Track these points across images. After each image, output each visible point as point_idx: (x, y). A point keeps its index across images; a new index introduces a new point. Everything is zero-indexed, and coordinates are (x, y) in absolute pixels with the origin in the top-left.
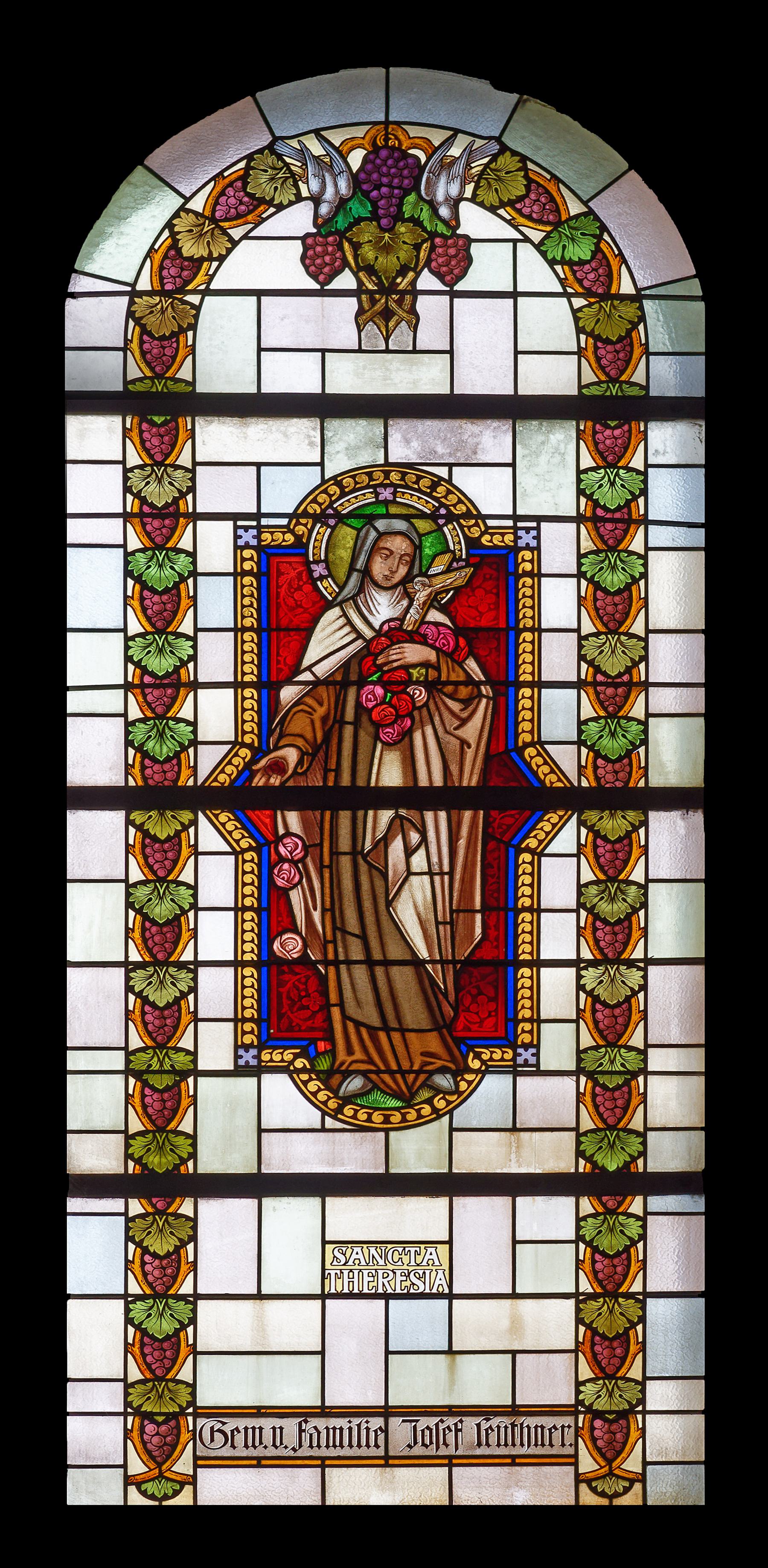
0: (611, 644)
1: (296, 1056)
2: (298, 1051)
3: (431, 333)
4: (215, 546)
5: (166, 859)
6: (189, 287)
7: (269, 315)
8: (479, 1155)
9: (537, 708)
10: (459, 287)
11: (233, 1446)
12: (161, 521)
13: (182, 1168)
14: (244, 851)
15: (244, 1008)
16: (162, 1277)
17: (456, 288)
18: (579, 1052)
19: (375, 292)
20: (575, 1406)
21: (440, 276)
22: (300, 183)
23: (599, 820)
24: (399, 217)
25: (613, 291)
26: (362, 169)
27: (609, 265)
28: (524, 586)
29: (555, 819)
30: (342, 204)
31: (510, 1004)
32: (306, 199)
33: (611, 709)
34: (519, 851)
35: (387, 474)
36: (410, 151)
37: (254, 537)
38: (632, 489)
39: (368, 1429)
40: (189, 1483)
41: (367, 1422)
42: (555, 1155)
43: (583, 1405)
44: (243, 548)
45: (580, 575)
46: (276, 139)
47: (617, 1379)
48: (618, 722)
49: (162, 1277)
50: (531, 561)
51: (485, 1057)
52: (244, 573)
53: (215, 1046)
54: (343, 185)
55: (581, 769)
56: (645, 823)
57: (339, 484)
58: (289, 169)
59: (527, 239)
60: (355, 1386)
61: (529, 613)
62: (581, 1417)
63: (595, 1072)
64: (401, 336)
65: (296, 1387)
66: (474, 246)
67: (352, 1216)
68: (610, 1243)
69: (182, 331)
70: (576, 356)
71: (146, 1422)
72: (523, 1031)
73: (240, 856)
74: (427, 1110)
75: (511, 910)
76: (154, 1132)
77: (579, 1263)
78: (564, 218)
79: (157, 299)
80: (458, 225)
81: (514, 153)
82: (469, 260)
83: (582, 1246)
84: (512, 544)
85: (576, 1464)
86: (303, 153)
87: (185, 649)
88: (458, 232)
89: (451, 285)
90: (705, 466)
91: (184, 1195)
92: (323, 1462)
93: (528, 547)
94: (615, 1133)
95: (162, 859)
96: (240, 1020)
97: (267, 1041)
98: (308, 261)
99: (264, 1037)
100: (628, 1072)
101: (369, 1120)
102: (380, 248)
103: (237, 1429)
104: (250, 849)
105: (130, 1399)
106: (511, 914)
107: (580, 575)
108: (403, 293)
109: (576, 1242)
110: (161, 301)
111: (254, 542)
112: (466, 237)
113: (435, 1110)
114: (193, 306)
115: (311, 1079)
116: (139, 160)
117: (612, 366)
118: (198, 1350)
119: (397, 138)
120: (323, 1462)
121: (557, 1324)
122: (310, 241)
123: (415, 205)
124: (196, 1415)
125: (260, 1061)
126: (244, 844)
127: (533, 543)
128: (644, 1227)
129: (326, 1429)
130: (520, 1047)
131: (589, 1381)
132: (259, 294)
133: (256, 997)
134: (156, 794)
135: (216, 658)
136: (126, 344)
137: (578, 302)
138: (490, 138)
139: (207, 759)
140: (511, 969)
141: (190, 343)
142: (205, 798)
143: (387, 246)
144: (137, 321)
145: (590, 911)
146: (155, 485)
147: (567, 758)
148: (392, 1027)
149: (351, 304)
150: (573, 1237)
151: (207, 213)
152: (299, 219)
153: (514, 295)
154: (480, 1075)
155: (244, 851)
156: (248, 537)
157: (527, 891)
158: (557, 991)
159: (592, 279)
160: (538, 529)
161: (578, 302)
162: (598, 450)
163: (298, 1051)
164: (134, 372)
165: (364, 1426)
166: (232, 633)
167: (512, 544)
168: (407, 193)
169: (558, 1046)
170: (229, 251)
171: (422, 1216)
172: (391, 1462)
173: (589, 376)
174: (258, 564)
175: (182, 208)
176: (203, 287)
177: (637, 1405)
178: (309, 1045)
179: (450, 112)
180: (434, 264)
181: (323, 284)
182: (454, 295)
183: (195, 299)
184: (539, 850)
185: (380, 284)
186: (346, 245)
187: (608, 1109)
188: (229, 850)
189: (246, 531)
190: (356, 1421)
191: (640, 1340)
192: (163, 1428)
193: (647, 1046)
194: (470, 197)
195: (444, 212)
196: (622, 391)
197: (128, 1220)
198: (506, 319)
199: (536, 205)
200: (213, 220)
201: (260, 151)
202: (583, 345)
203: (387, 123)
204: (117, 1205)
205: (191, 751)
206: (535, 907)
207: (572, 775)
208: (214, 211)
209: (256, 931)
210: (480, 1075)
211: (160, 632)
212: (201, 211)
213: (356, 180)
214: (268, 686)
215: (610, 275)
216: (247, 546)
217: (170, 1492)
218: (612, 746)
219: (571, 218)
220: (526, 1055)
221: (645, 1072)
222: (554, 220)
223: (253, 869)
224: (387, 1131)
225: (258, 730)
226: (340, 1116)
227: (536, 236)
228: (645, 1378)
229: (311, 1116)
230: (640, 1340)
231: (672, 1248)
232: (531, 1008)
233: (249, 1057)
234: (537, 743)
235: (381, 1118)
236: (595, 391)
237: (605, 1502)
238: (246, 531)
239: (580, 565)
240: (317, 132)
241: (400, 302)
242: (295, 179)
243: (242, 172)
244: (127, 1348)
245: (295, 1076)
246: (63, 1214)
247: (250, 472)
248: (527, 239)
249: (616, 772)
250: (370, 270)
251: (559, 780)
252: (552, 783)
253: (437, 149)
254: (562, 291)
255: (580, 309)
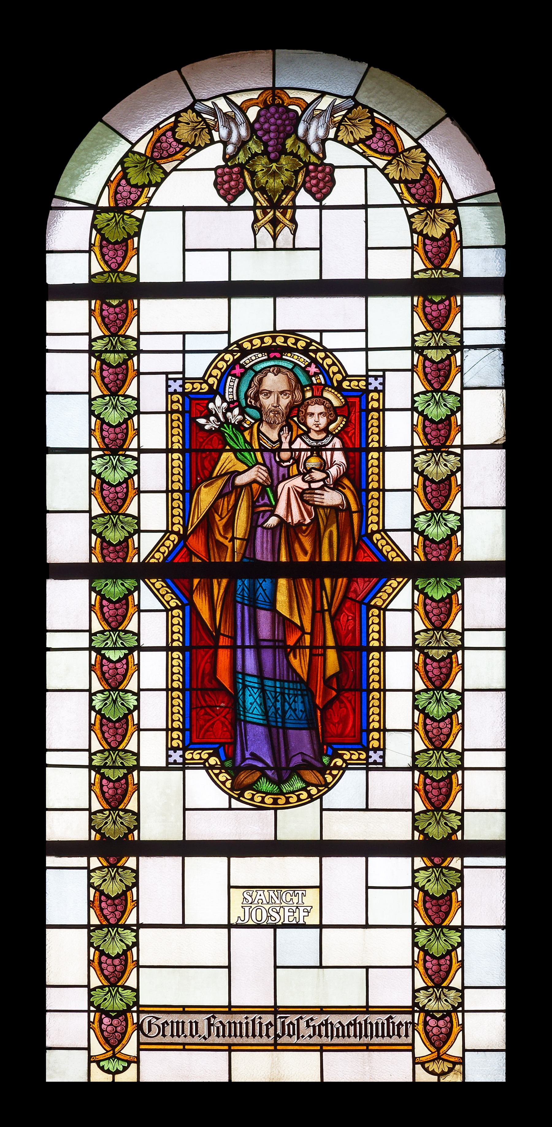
0: (436, 875)
1: (210, 755)
2: (211, 751)
3: (306, 235)
4: (152, 393)
5: (117, 910)
6: (136, 205)
7: (191, 226)
8: (341, 828)
9: (382, 666)
10: (327, 202)
11: (164, 1035)
12: (114, 369)
13: (130, 837)
14: (172, 609)
15: (173, 721)
16: (113, 911)
17: (323, 203)
18: (414, 634)
19: (267, 207)
20: (412, 1007)
21: (313, 195)
22: (213, 131)
23: (428, 1002)
24: (283, 151)
25: (436, 202)
26: (257, 120)
27: (433, 184)
28: (372, 418)
29: (394, 584)
30: (242, 144)
31: (364, 717)
32: (218, 142)
33: (436, 262)
34: (369, 607)
35: (275, 801)
36: (290, 107)
37: (180, 386)
38: (451, 883)
39: (261, 1024)
40: (134, 1062)
41: (260, 1018)
42: (400, 829)
43: (418, 1007)
44: (172, 394)
45: (413, 409)
46: (195, 101)
47: (442, 392)
48: (442, 930)
49: (113, 911)
50: (379, 740)
51: (346, 757)
52: (173, 412)
53: (152, 748)
54: (243, 132)
55: (414, 548)
56: (462, 588)
57: (240, 346)
58: (205, 122)
59: (374, 166)
60: (253, 993)
61: (376, 438)
62: (416, 1015)
63: (426, 768)
64: (285, 238)
65: (209, 991)
66: (336, 170)
67: (249, 869)
68: (436, 413)
69: (130, 237)
70: (410, 373)
71: (103, 1016)
72: (372, 399)
73: (170, 612)
74: (304, 795)
75: (364, 690)
76: (109, 336)
77: (414, 904)
78: (400, 150)
79: (112, 214)
80: (325, 157)
81: (364, 107)
82: (333, 182)
83: (416, 891)
84: (365, 388)
85: (413, 1051)
86: (214, 112)
87: (130, 465)
88: (325, 161)
89: (320, 200)
90: (503, 348)
91: (129, 855)
92: (230, 1048)
93: (376, 390)
94: (440, 271)
95: (114, 614)
96: (170, 491)
97: (189, 745)
98: (219, 186)
99: (187, 742)
100: (450, 768)
101: (263, 801)
102: (271, 174)
103: (166, 1022)
104: (177, 607)
105: (93, 468)
106: (364, 694)
107: (413, 409)
108: (286, 208)
109: (412, 888)
110: (115, 216)
111: (180, 390)
112: (331, 165)
113: (310, 795)
114: (137, 219)
115: (221, 773)
116: (98, 118)
117: (436, 976)
118: (140, 964)
119: (280, 98)
120: (230, 1048)
121: (399, 947)
122: (219, 171)
123: (294, 144)
124: (139, 1012)
125: (185, 759)
126: (173, 604)
127: (380, 388)
128: (462, 820)
129: (230, 1026)
130: (371, 750)
131: (423, 691)
132: (184, 209)
133: (181, 435)
134: (111, 567)
135: (153, 472)
136: (90, 247)
137: (411, 211)
138: (347, 98)
139: (147, 543)
140: (364, 654)
141: (136, 246)
142: (145, 571)
143: (275, 172)
144: (99, 231)
145: (422, 889)
146: (110, 470)
147: (404, 541)
148: (277, 714)
149: (249, 215)
150: (410, 884)
151: (149, 154)
152: (212, 156)
153: (365, 207)
154: (341, 771)
155: (172, 609)
156: (176, 386)
157: (376, 628)
158: (399, 711)
159: (422, 193)
160: (384, 376)
161: (411, 211)
162: (427, 318)
163: (211, 751)
164: (96, 269)
165: (257, 1021)
166: (165, 415)
167: (365, 388)
168: (289, 136)
169: (399, 749)
170: (163, 180)
171: (301, 869)
172: (279, 1047)
173: (419, 265)
174: (183, 405)
175: (130, 151)
176: (145, 205)
177: (458, 1007)
178: (219, 748)
179: (318, 82)
180: (308, 185)
181: (229, 202)
182: (321, 208)
183: (138, 214)
184: (383, 607)
185: (270, 200)
186: (246, 173)
187: (435, 615)
188: (163, 608)
189: (175, 381)
190: (252, 1017)
191: (460, 602)
192: (115, 1022)
193: (464, 750)
194: (333, 137)
195: (315, 147)
196: (442, 275)
197: (90, 871)
198: (360, 224)
199: (381, 143)
200: (152, 158)
201: (185, 110)
202: (415, 242)
203: (273, 88)
204: (82, 861)
205: (135, 418)
206: (381, 488)
207: (408, 551)
208: (153, 152)
209: (181, 428)
210: (341, 771)
211: (114, 630)
212: (144, 153)
213: (251, 127)
214: (189, 492)
215: (434, 190)
216: (175, 392)
217: (121, 1068)
218: (437, 532)
219: (405, 150)
220: (375, 757)
221: (463, 648)
222: (395, 153)
223: (179, 399)
224: (276, 810)
225: (182, 408)
226: (241, 798)
227: (381, 164)
228: (464, 987)
229: (221, 799)
230: (461, 1022)
231: (485, 891)
232: (379, 722)
233: (176, 756)
234: (382, 530)
235: (271, 801)
236: (422, 275)
237: (434, 1079)
238: (175, 381)
239: (413, 402)
240: (225, 95)
241: (284, 214)
242: (210, 129)
243: (172, 125)
244: (90, 904)
245: (210, 771)
246: (44, 868)
247: (179, 338)
248: (374, 166)
249: (440, 668)
250: (263, 190)
251: (398, 555)
252: (393, 558)
253: (309, 105)
254: (400, 203)
255: (412, 216)
